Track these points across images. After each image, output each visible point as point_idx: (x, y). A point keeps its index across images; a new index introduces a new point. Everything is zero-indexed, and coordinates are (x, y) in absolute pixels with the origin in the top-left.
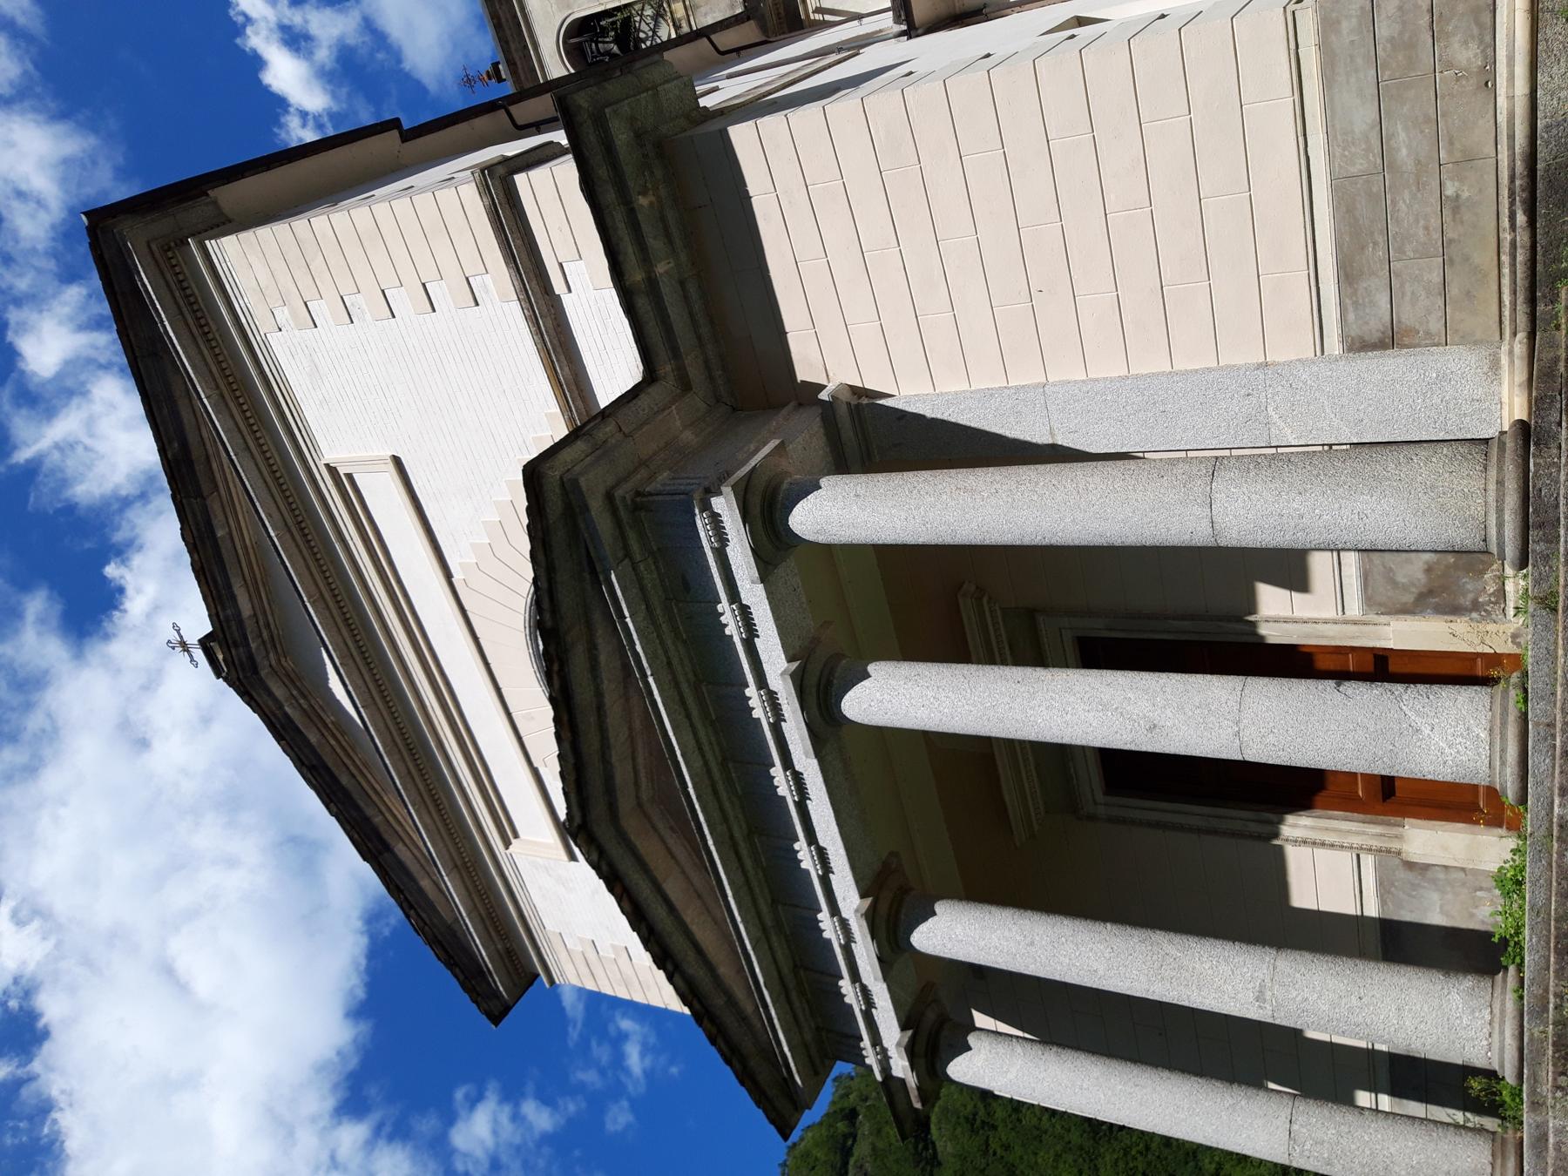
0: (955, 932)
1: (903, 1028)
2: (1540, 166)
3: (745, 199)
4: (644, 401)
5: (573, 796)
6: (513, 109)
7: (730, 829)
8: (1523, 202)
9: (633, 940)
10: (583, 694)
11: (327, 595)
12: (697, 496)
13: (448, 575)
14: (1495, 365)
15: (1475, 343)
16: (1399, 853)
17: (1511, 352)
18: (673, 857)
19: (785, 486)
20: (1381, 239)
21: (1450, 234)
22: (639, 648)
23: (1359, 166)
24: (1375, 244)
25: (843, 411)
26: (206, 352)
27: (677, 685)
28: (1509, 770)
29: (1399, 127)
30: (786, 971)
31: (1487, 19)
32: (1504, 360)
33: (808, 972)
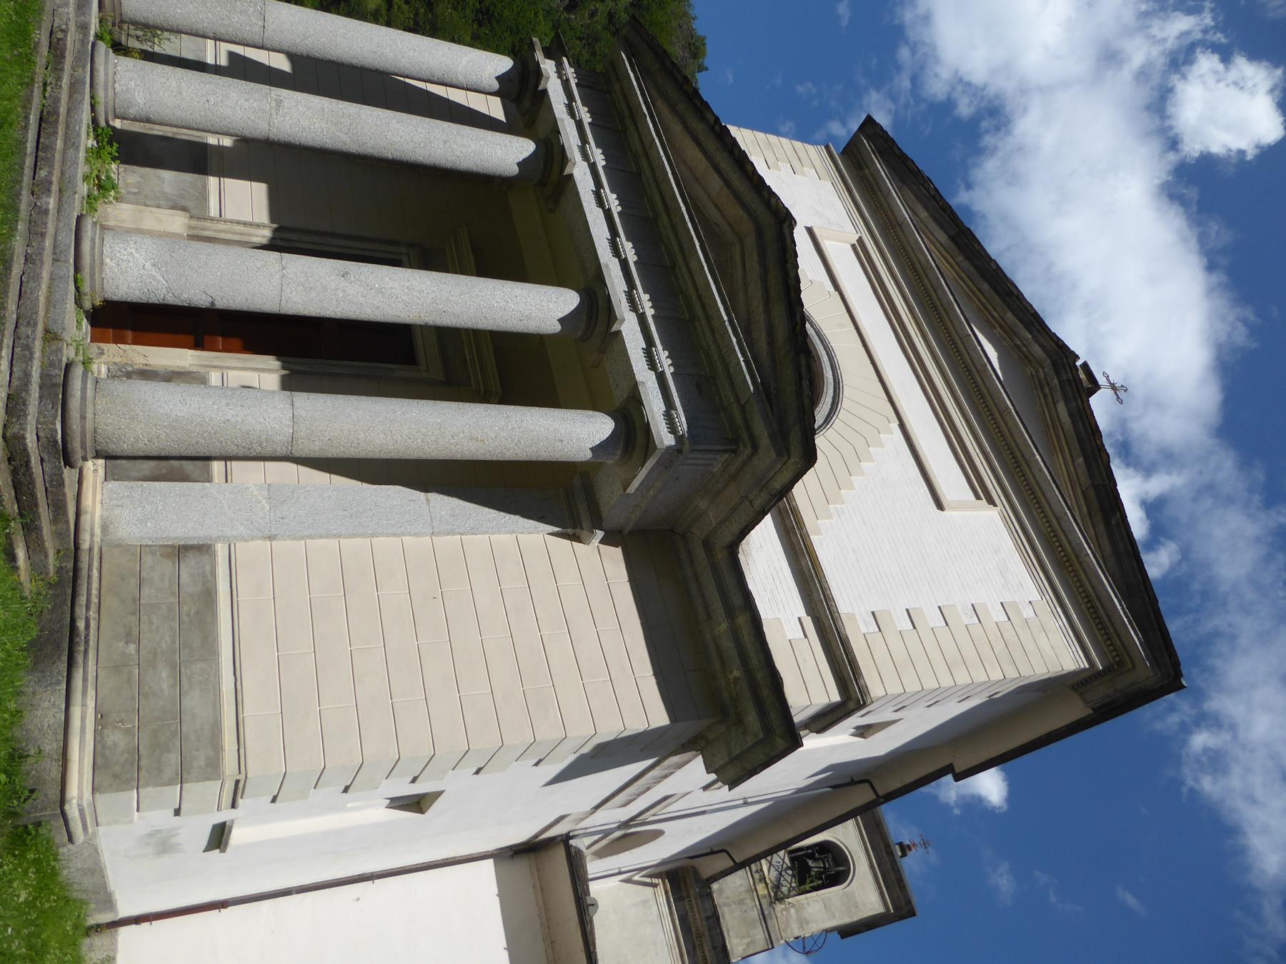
0: (506, 153)
1: (545, 92)
2: (65, 658)
3: (658, 673)
4: (735, 528)
5: (789, 241)
6: (872, 796)
7: (670, 220)
8: (78, 635)
9: (761, 169)
10: (779, 311)
11: (997, 415)
12: (687, 446)
13: (902, 426)
14: (105, 528)
15: (119, 546)
16: (191, 217)
17: (92, 535)
18: (716, 206)
19: (619, 452)
20: (185, 618)
21: (134, 619)
22: (734, 340)
23: (197, 667)
24: (188, 615)
25: (586, 523)
26: (1089, 588)
27: (708, 318)
28: (89, 234)
29: (166, 692)
30: (632, 129)
31: (99, 761)
32: (98, 531)
33: (614, 125)
